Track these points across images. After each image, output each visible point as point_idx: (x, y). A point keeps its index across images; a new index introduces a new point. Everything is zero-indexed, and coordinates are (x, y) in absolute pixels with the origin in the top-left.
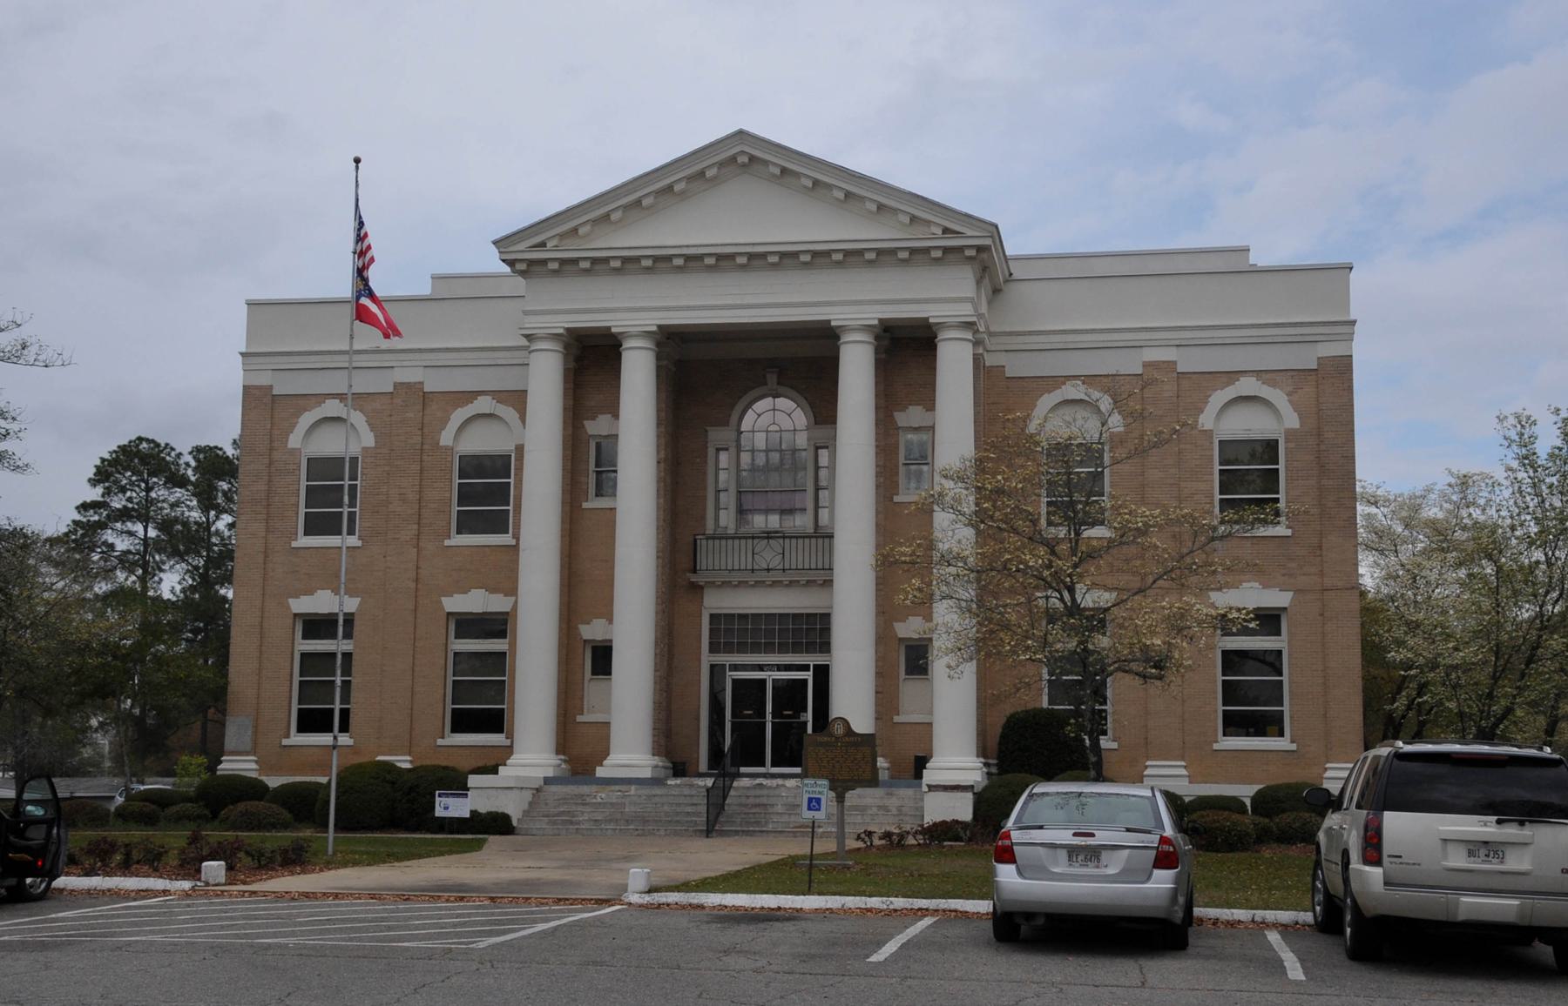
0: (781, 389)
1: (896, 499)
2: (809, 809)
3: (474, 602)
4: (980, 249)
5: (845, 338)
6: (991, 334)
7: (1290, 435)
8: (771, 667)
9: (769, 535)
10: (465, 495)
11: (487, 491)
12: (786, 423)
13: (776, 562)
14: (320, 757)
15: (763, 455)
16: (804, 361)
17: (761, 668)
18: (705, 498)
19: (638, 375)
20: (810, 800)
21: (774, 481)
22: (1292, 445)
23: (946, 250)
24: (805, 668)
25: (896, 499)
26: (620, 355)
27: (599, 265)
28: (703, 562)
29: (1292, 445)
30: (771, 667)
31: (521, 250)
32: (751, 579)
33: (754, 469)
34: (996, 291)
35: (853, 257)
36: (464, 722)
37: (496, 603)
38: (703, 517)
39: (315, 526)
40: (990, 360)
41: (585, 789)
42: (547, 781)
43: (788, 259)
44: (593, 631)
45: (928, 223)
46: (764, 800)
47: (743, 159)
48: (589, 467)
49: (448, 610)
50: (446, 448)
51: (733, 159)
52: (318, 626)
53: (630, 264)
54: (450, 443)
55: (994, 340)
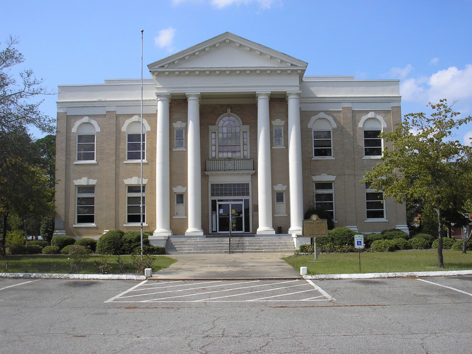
0: (232, 114)
2: (358, 245)
8: (230, 200)
9: (229, 159)
10: (367, 143)
11: (135, 146)
15: (226, 134)
16: (244, 107)
17: (227, 200)
19: (193, 108)
20: (358, 242)
21: (229, 142)
24: (242, 200)
30: (230, 200)
31: (156, 69)
33: (223, 138)
35: (263, 72)
37: (92, 182)
39: (131, 156)
41: (182, 239)
44: (178, 190)
48: (176, 138)
51: (225, 41)
52: (132, 189)
53: (192, 73)
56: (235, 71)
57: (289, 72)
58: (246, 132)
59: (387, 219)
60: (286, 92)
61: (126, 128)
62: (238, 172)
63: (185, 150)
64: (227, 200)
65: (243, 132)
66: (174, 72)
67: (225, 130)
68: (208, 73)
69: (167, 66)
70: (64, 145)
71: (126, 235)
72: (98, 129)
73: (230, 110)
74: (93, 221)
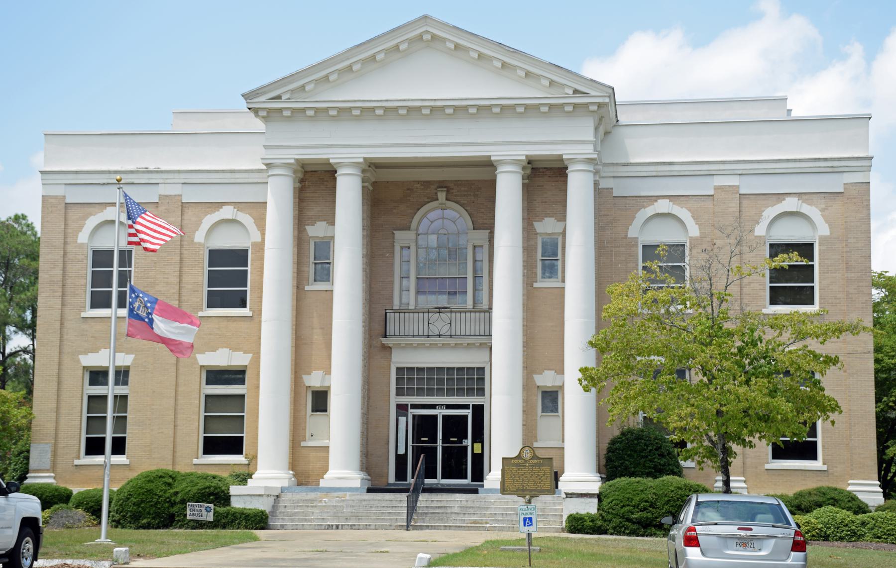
0: (449, 203)
1: (535, 285)
3: (221, 359)
4: (600, 105)
5: (500, 169)
6: (605, 165)
7: (823, 240)
10: (213, 279)
11: (229, 276)
12: (452, 228)
13: (445, 330)
14: (109, 475)
16: (470, 187)
17: (433, 407)
18: (392, 282)
19: (349, 194)
22: (824, 248)
23: (575, 106)
24: (466, 407)
25: (535, 285)
26: (335, 179)
27: (321, 114)
28: (391, 329)
29: (824, 248)
30: (441, 406)
31: (261, 102)
32: (427, 341)
34: (607, 133)
35: (507, 111)
36: (212, 446)
37: (238, 360)
38: (391, 298)
40: (604, 184)
41: (312, 495)
42: (283, 489)
43: (460, 111)
44: (546, 380)
45: (563, 86)
46: (442, 504)
47: (427, 37)
48: (312, 261)
49: (201, 364)
50: (200, 244)
51: (420, 37)
53: (344, 113)
54: (202, 241)
55: (606, 169)
56: (443, 108)
57: (569, 109)
58: (482, 246)
59: (824, 464)
60: (562, 155)
61: (767, 229)
62: (459, 340)
63: (559, 285)
64: (433, 407)
65: (402, 248)
66: (304, 110)
67: (433, 240)
68: (379, 112)
69: (288, 96)
70: (58, 272)
71: (184, 484)
72: (694, 230)
73: (444, 194)
74: (240, 452)
